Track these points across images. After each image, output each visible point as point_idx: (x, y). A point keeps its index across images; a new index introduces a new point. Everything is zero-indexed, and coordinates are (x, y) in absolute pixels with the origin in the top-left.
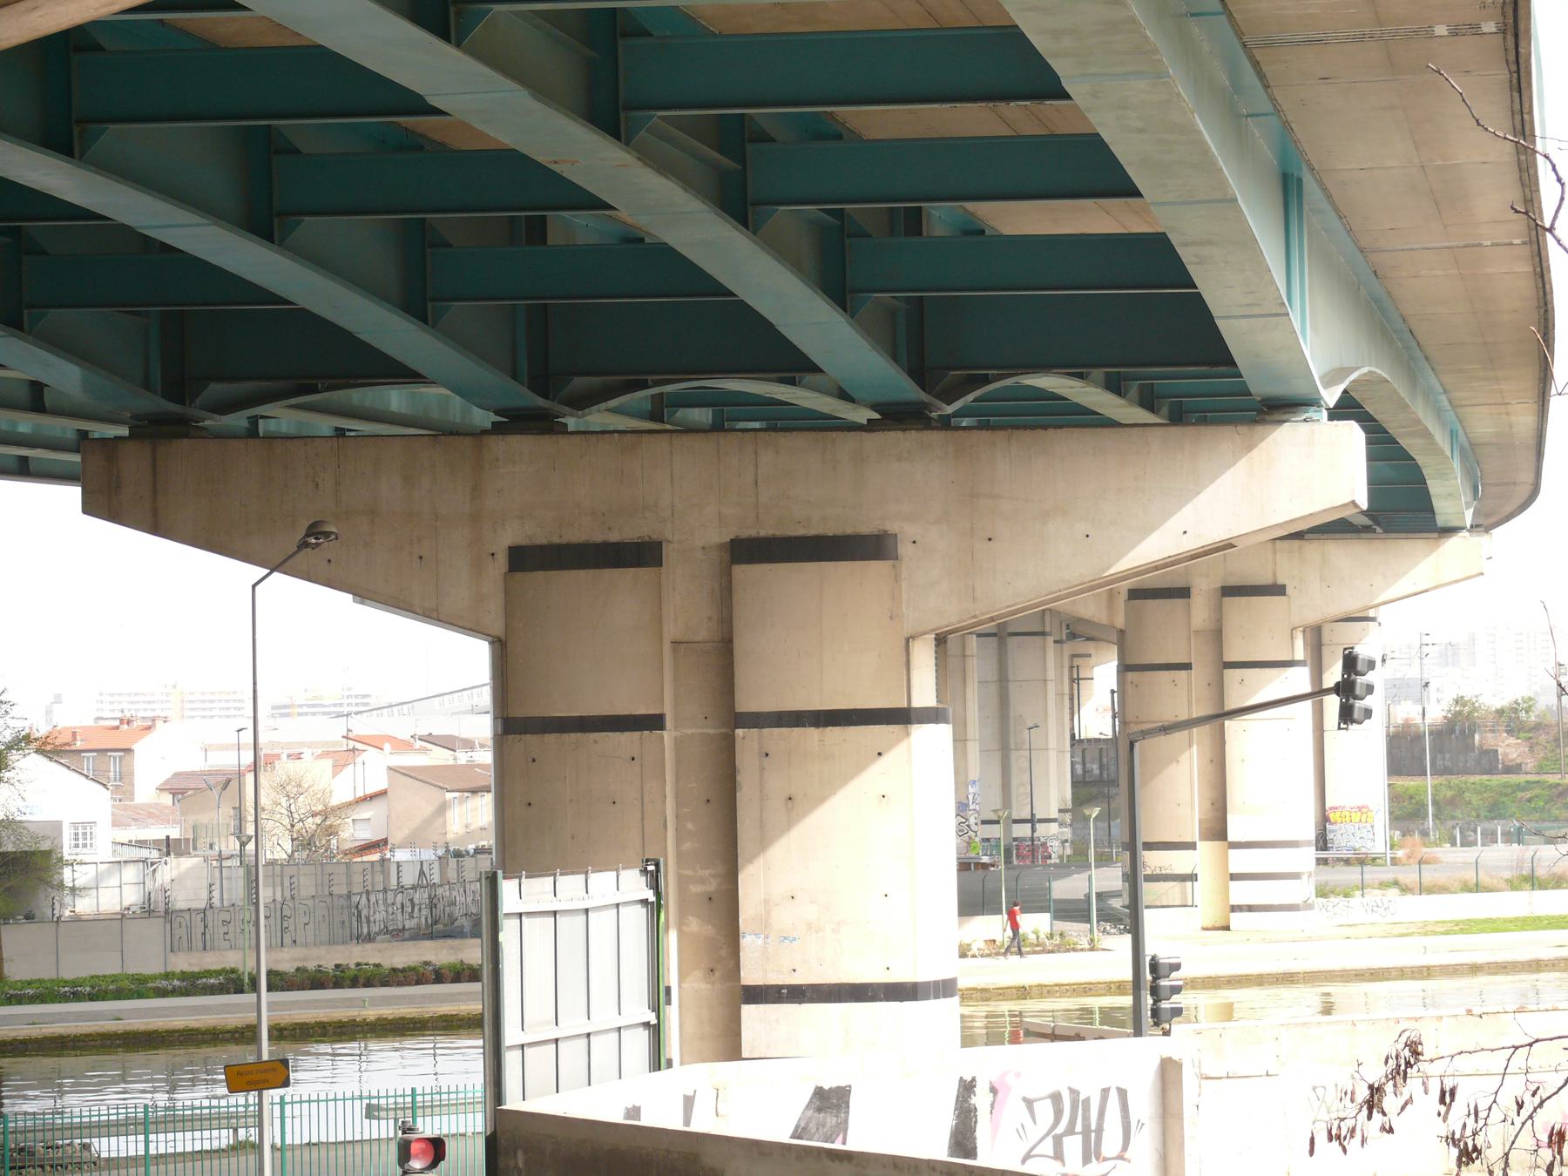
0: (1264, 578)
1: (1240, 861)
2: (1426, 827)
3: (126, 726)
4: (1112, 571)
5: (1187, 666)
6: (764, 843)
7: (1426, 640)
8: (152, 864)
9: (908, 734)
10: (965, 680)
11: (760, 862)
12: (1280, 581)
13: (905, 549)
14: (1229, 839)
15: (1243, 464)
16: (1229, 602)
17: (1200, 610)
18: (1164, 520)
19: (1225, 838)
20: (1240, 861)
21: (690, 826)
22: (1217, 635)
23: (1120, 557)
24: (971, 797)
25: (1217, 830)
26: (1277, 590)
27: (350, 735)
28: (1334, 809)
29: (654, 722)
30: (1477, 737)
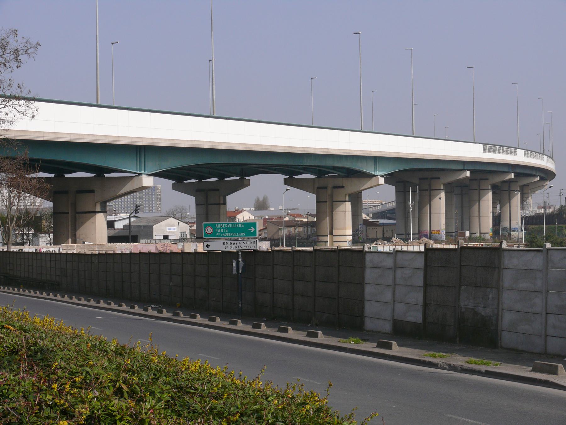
0: (341, 185)
1: (336, 239)
2: (287, 230)
3: (236, 211)
4: (118, 194)
5: (326, 202)
6: (79, 228)
7: (562, 191)
8: (183, 240)
9: (96, 215)
10: (358, 202)
11: (79, 230)
12: (343, 186)
13: (95, 192)
14: (334, 234)
15: (131, 182)
16: (334, 189)
17: (329, 191)
18: (123, 188)
19: (333, 234)
20: (336, 239)
21: (447, 343)
22: (332, 196)
23: (118, 193)
24: (359, 228)
25: (331, 233)
26: (343, 187)
27: (288, 214)
28: (433, 231)
29: (68, 213)
30: (564, 215)
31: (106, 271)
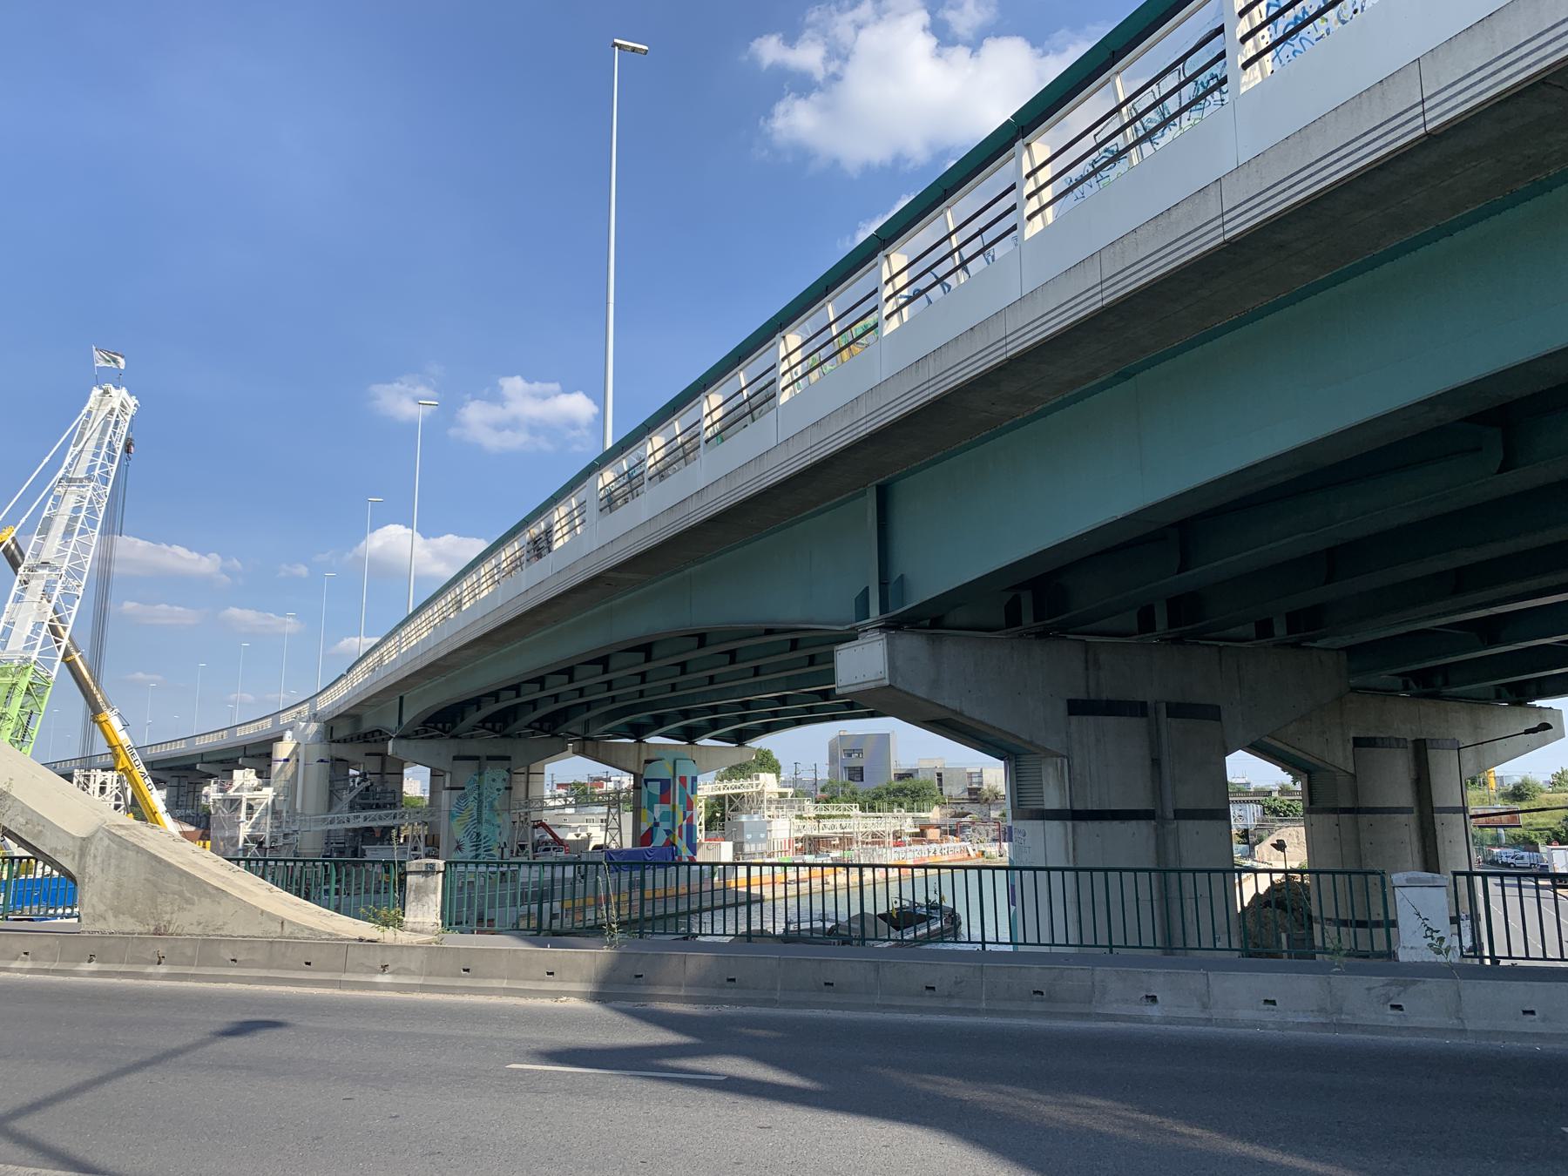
31: (529, 774)
